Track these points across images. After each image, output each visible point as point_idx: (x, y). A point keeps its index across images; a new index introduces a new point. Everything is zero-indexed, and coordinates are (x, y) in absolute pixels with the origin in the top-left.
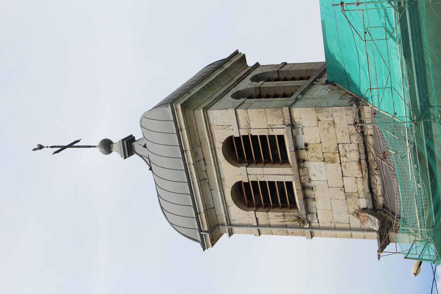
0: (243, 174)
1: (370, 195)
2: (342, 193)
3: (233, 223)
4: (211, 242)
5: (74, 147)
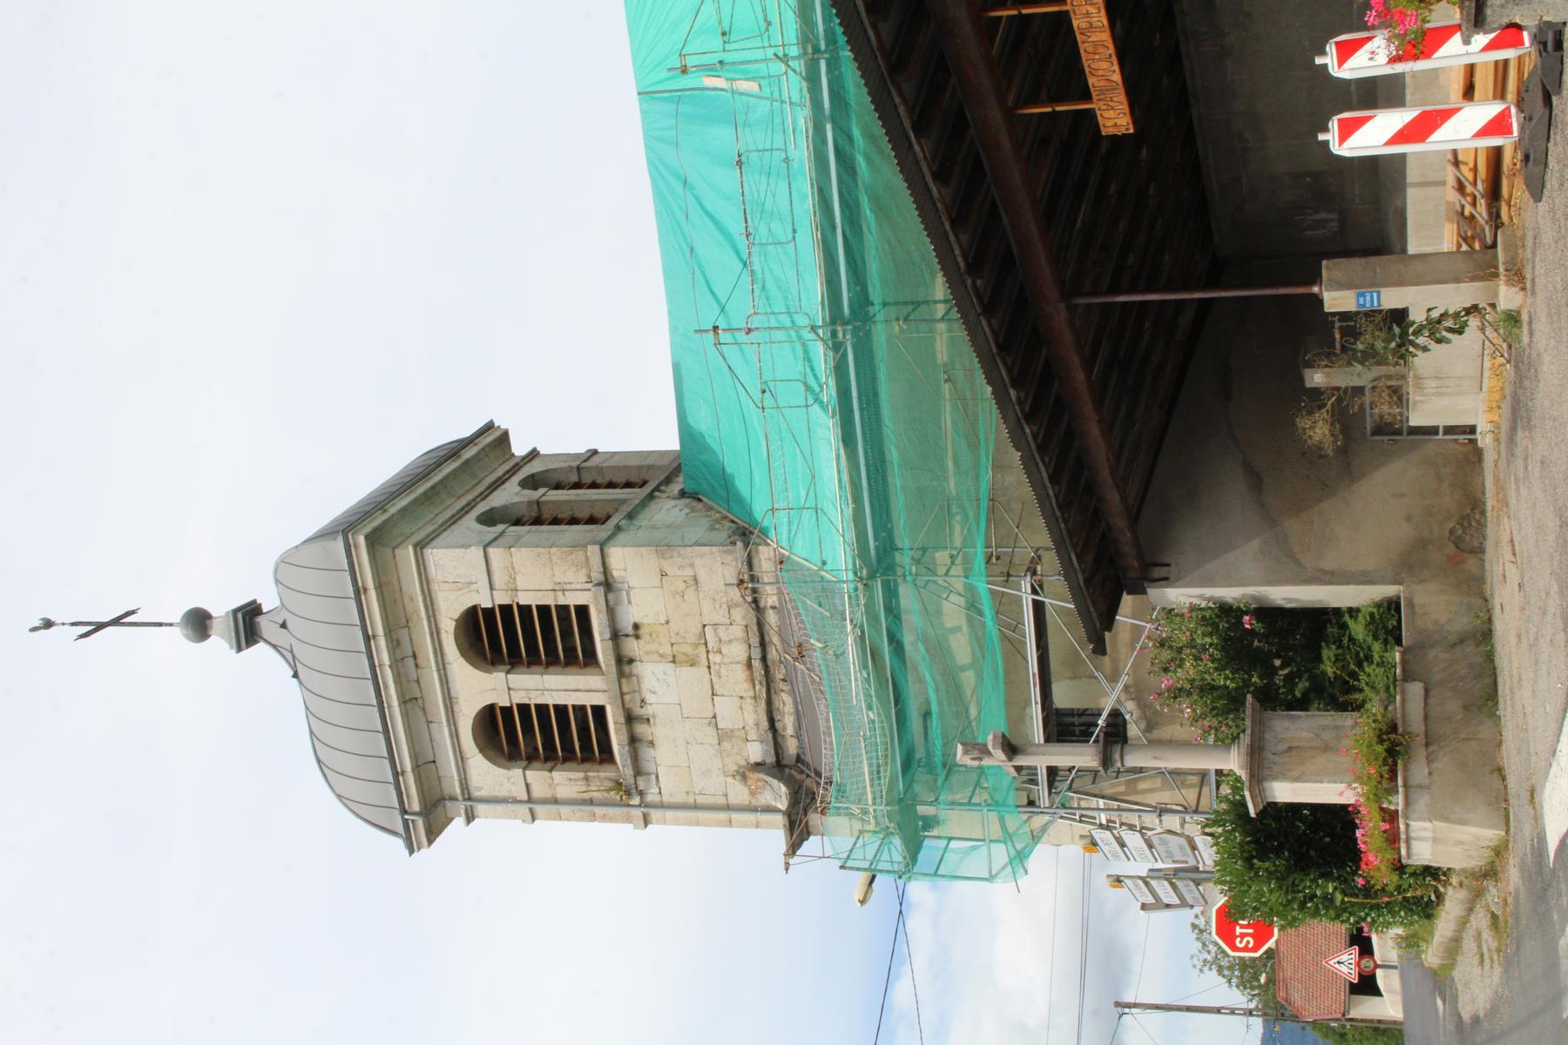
2: (711, 731)
3: (476, 794)
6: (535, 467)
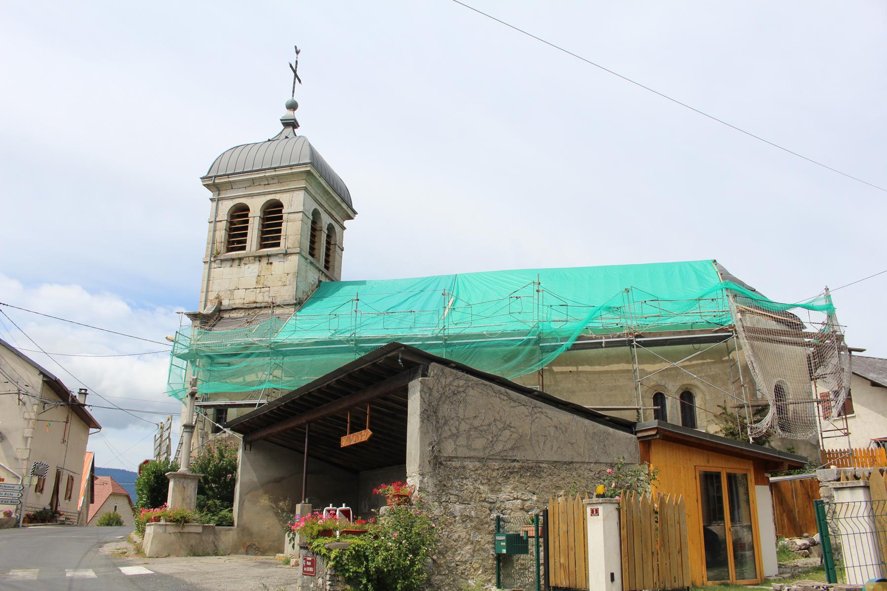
3: (220, 202)
6: (337, 228)
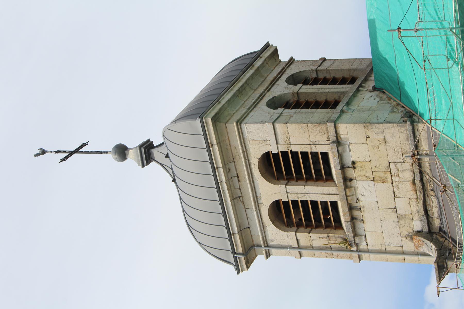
0: (281, 192)
1: (425, 218)
2: (394, 215)
3: (271, 243)
4: (246, 264)
5: (82, 152)
